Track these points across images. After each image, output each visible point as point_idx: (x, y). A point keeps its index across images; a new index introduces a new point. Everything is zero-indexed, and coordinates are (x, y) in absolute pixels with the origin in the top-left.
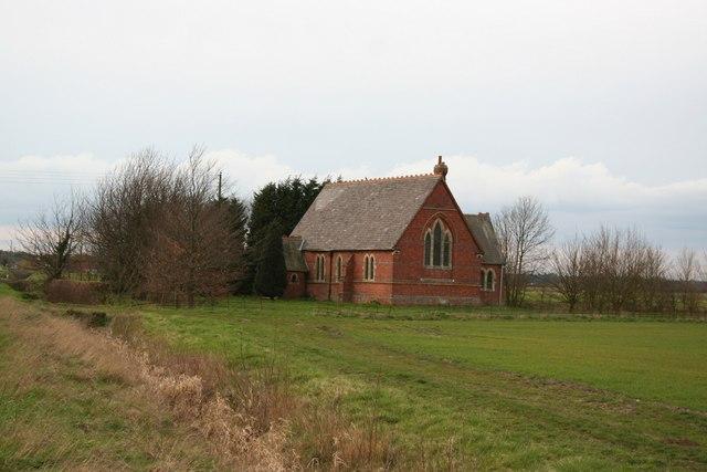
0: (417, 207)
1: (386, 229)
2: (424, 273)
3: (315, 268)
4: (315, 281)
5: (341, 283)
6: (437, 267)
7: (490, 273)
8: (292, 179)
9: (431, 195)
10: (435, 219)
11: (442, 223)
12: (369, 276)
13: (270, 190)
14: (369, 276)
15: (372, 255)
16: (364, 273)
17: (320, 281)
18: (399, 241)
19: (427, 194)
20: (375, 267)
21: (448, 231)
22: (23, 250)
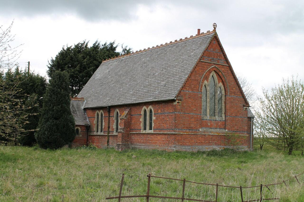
0: (195, 61)
1: (163, 83)
2: (202, 123)
3: (95, 122)
4: (95, 133)
5: (120, 135)
6: (213, 118)
7: (145, 129)
8: (93, 44)
9: (207, 49)
10: (210, 72)
11: (215, 75)
12: (148, 127)
13: (118, 52)
14: (148, 127)
15: (150, 107)
16: (142, 125)
17: (99, 133)
18: (180, 92)
19: (204, 47)
20: (154, 118)
21: (221, 84)
22: (244, 91)
